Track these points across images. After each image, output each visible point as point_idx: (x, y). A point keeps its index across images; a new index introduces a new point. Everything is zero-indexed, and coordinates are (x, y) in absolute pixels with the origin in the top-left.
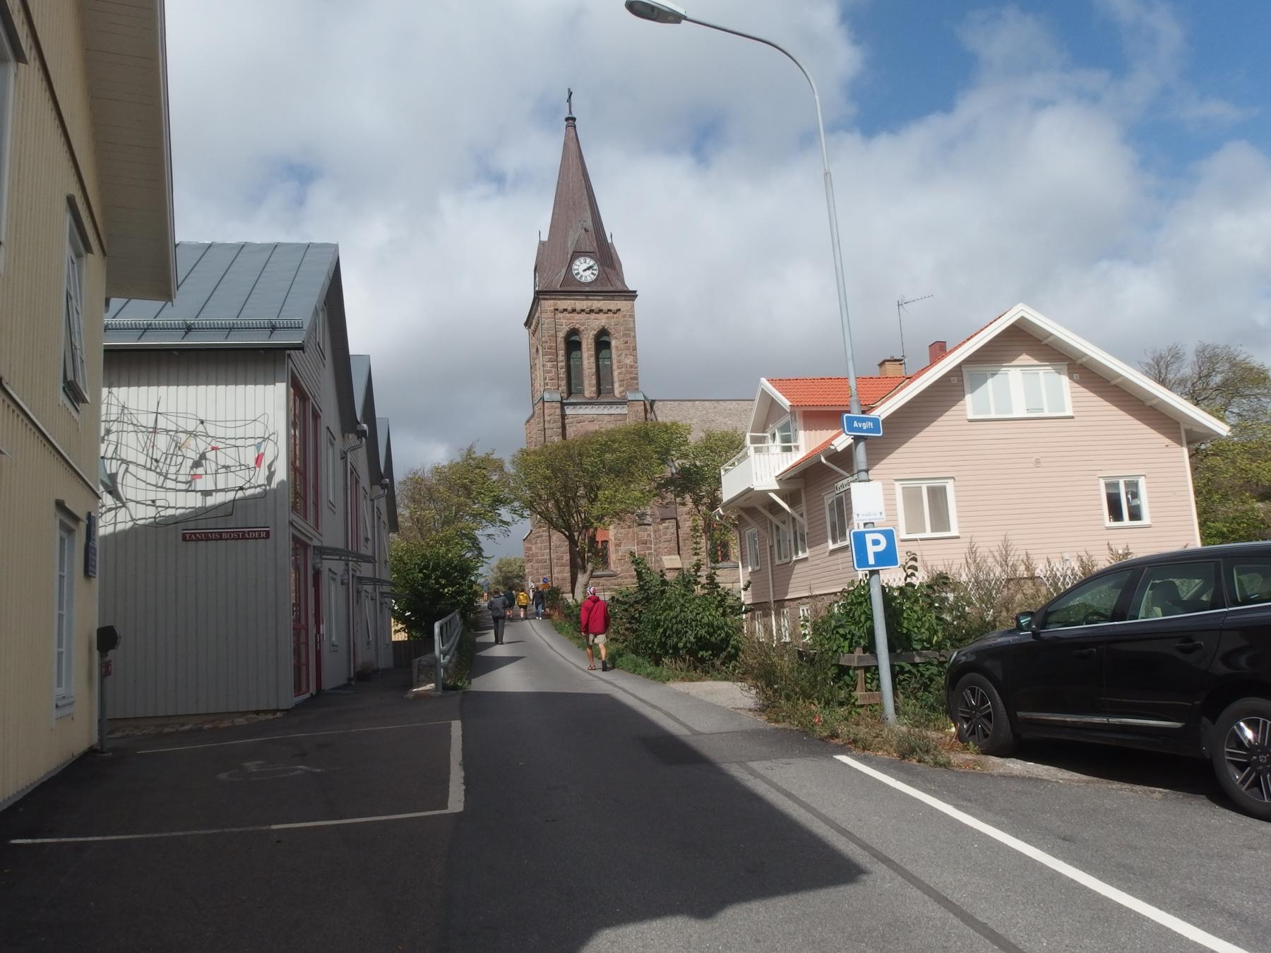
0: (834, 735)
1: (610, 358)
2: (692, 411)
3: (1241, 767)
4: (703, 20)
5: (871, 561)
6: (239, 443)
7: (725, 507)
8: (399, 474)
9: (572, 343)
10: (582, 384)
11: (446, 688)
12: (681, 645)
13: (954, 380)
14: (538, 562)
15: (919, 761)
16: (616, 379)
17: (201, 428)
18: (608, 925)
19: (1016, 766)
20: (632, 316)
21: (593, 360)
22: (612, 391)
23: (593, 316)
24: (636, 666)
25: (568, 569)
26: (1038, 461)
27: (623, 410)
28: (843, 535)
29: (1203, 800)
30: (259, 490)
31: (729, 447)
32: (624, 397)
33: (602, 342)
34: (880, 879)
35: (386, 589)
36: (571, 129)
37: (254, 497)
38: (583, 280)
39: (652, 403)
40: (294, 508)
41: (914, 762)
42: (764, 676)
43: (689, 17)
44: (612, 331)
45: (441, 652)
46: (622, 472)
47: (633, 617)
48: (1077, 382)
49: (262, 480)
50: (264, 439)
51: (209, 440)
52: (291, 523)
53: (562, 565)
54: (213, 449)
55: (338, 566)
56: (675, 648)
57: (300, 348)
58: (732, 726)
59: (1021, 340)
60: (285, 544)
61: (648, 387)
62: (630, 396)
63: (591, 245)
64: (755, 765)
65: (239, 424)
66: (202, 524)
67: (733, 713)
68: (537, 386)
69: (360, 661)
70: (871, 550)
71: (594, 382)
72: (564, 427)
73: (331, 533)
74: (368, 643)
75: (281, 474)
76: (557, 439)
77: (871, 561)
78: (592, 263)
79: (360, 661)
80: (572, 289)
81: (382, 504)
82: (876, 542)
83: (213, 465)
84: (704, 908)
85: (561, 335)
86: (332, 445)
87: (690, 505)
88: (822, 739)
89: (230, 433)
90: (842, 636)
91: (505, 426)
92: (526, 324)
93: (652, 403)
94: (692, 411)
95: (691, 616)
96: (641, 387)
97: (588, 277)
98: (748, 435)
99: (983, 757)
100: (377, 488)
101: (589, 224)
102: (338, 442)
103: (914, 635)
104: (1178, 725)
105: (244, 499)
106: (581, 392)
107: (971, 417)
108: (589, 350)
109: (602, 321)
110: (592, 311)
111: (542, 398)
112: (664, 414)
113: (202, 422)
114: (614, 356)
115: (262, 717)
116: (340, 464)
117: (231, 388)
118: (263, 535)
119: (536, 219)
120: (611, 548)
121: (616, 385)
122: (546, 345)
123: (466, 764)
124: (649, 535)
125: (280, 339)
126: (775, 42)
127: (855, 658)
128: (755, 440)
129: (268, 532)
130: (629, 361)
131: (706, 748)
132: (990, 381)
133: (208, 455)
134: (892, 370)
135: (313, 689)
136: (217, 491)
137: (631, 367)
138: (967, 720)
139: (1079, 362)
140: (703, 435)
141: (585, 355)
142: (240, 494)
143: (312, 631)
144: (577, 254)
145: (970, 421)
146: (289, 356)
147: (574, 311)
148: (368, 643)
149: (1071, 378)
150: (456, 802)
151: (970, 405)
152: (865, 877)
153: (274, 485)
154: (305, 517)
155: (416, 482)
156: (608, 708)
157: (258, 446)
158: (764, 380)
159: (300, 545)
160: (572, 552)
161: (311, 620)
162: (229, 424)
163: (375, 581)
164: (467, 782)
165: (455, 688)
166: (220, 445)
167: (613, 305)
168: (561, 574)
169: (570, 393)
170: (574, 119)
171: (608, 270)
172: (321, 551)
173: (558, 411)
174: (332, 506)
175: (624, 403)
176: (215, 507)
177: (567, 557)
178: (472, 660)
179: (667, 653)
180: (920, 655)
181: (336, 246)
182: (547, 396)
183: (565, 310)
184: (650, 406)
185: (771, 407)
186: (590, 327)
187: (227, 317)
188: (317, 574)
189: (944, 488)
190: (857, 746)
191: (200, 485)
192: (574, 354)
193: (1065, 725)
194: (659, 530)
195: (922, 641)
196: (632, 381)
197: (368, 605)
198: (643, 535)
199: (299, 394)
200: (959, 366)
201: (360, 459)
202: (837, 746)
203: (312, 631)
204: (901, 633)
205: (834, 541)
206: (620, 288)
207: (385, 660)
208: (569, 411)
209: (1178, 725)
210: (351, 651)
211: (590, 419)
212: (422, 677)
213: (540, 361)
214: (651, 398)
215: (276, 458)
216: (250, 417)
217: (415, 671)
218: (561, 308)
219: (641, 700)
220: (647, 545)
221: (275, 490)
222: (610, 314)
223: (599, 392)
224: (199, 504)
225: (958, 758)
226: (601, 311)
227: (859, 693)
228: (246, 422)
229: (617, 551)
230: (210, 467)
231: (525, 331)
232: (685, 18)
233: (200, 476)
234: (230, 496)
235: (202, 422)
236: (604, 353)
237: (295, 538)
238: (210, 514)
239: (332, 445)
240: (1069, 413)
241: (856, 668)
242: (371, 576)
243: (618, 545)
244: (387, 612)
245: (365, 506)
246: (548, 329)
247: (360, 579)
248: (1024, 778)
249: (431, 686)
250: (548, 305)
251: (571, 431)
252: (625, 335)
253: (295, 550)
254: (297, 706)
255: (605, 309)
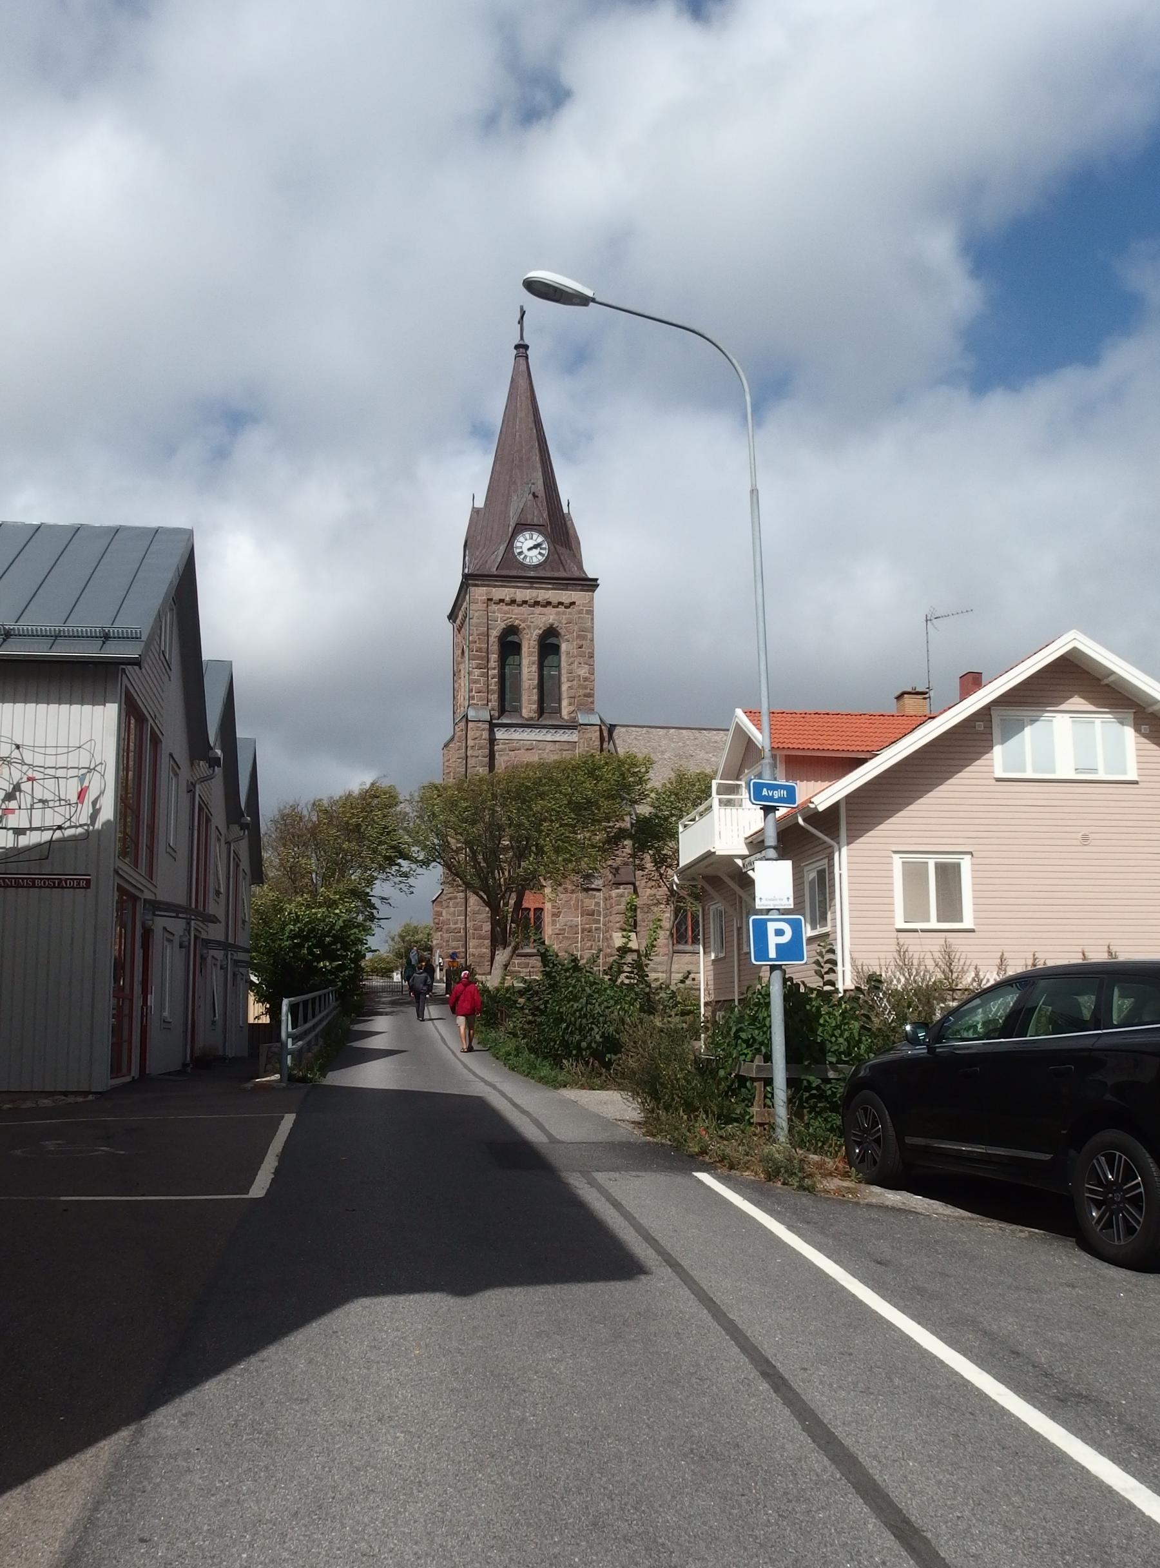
0: (703, 1152)
1: (559, 667)
2: (664, 742)
3: (1098, 1205)
4: (614, 304)
5: (772, 953)
6: (60, 773)
7: (682, 873)
8: (269, 806)
9: (509, 644)
10: (519, 700)
11: (291, 1079)
12: (584, 1044)
13: (980, 726)
14: (449, 931)
15: (784, 1184)
16: (564, 695)
17: (16, 754)
18: (366, 1295)
19: (894, 1198)
20: (590, 612)
21: (535, 668)
22: (558, 710)
23: (538, 610)
24: (533, 1067)
25: (487, 942)
26: (1085, 838)
27: (573, 736)
28: (824, 918)
29: (1071, 1242)
30: (80, 830)
31: (691, 794)
32: (574, 720)
33: (549, 644)
34: (661, 1278)
35: (242, 956)
36: (522, 361)
37: (74, 839)
38: (527, 561)
39: (612, 728)
40: (123, 854)
41: (779, 1184)
42: (649, 1086)
43: (598, 299)
44: (562, 632)
45: (289, 1036)
46: (584, 811)
47: (537, 1009)
48: (1145, 736)
49: (84, 819)
50: (90, 770)
51: (25, 768)
52: (116, 872)
53: (481, 937)
54: (29, 779)
55: (177, 926)
56: (578, 1047)
57: (136, 662)
58: (601, 1137)
59: (1071, 678)
60: (108, 897)
61: (606, 709)
62: (582, 719)
63: (540, 515)
64: (600, 1177)
65: (60, 750)
66: (12, 868)
67: (614, 1123)
68: (460, 699)
69: (201, 1041)
70: (773, 941)
71: (535, 697)
72: (492, 756)
73: (170, 882)
74: (214, 1023)
75: (107, 812)
76: (483, 771)
77: (772, 953)
78: (540, 539)
79: (201, 1041)
80: (511, 573)
81: (243, 848)
82: (780, 933)
83: (29, 798)
84: (464, 1283)
85: (495, 633)
86: (176, 775)
87: (649, 865)
88: (691, 1156)
89: (50, 762)
90: (745, 1041)
91: (416, 753)
92: (452, 616)
93: (612, 728)
94: (664, 742)
95: (598, 1010)
96: (597, 707)
97: (534, 557)
98: (714, 783)
99: (863, 1186)
100: (235, 828)
101: (539, 488)
102: (185, 773)
103: (829, 1045)
104: (1048, 1157)
105: (63, 840)
106: (517, 710)
107: (999, 774)
108: (530, 655)
109: (549, 617)
110: (537, 603)
111: (466, 716)
112: (626, 744)
113: (18, 747)
114: (564, 664)
115: (71, 1099)
116: (185, 799)
117: (53, 707)
118: (83, 884)
119: (462, 483)
120: (547, 918)
121: (565, 703)
122: (475, 646)
123: (282, 1157)
124: (598, 904)
125: (114, 651)
126: (701, 332)
127: (751, 1068)
128: (724, 790)
129: (88, 881)
130: (583, 672)
131: (556, 1158)
132: (1028, 730)
133: (23, 787)
134: (916, 700)
135: (135, 1072)
136: (31, 829)
137: (586, 679)
138: (859, 1144)
139: (1150, 710)
140: (673, 775)
141: (525, 662)
142: (58, 834)
143: (138, 1002)
144: (522, 527)
145: (998, 780)
146: (123, 670)
147: (513, 602)
148: (214, 1023)
149: (1137, 730)
150: (259, 1188)
151: (999, 759)
152: (642, 1277)
153: (98, 825)
154: (136, 864)
155: (290, 820)
156: (477, 1111)
157: (82, 778)
158: (739, 712)
159: (127, 898)
160: (495, 923)
161: (138, 988)
162: (49, 751)
163: (225, 946)
164: (277, 1171)
165: (304, 1080)
166: (37, 775)
167: (566, 596)
168: (478, 948)
169: (502, 711)
170: (526, 347)
171: (561, 550)
172: (156, 906)
173: (486, 735)
174: (172, 852)
175: (574, 728)
176: (28, 849)
177: (487, 927)
178: (340, 1046)
179: (570, 1055)
180: (836, 1070)
181: (190, 534)
182: (472, 714)
183: (502, 601)
184: (608, 732)
185: (747, 751)
186: (533, 623)
187: (51, 624)
188: (147, 933)
189: (959, 865)
190: (726, 1167)
191: (12, 821)
192: (510, 660)
193: (959, 1157)
194: (610, 897)
195: (837, 1053)
196: (586, 700)
197: (215, 977)
198: (590, 903)
199: (134, 717)
200: (987, 709)
201: (214, 793)
202: (704, 1163)
203: (138, 1002)
204: (815, 1041)
205: (814, 928)
206: (577, 574)
207: (236, 1047)
208: (500, 734)
209: (1048, 1157)
210: (191, 1031)
211: (529, 746)
212: (269, 1067)
213: (465, 667)
214: (609, 721)
215: (102, 793)
216: (74, 742)
217: (263, 1059)
218: (496, 598)
219: (515, 1105)
220: (578, 920)
221: (99, 832)
222: (561, 609)
223: (541, 711)
224: (10, 845)
225: (834, 1184)
226: (549, 603)
227: (754, 1110)
228: (69, 749)
229: (554, 923)
230: (25, 799)
231: (449, 626)
232: (593, 300)
233: (12, 811)
234: (46, 836)
235: (18, 747)
236: (550, 660)
237: (120, 888)
238: (22, 857)
239: (176, 775)
240: (1132, 775)
241: (753, 1080)
242: (222, 939)
243: (555, 915)
244: (242, 985)
245: (217, 850)
246: (477, 625)
247: (207, 943)
248: (899, 1210)
249: (277, 1077)
250: (479, 593)
251: (501, 762)
252: (579, 637)
253: (120, 902)
254: (114, 1090)
255: (555, 601)
